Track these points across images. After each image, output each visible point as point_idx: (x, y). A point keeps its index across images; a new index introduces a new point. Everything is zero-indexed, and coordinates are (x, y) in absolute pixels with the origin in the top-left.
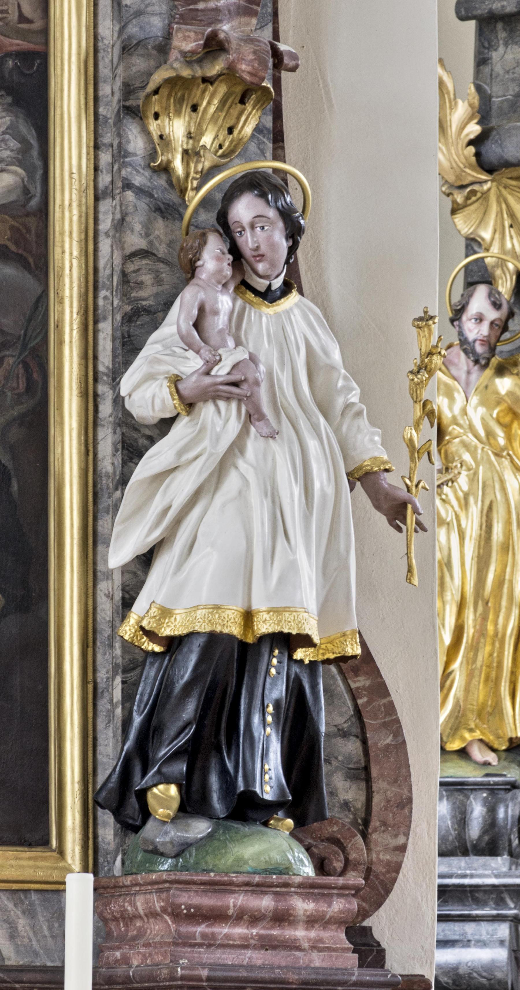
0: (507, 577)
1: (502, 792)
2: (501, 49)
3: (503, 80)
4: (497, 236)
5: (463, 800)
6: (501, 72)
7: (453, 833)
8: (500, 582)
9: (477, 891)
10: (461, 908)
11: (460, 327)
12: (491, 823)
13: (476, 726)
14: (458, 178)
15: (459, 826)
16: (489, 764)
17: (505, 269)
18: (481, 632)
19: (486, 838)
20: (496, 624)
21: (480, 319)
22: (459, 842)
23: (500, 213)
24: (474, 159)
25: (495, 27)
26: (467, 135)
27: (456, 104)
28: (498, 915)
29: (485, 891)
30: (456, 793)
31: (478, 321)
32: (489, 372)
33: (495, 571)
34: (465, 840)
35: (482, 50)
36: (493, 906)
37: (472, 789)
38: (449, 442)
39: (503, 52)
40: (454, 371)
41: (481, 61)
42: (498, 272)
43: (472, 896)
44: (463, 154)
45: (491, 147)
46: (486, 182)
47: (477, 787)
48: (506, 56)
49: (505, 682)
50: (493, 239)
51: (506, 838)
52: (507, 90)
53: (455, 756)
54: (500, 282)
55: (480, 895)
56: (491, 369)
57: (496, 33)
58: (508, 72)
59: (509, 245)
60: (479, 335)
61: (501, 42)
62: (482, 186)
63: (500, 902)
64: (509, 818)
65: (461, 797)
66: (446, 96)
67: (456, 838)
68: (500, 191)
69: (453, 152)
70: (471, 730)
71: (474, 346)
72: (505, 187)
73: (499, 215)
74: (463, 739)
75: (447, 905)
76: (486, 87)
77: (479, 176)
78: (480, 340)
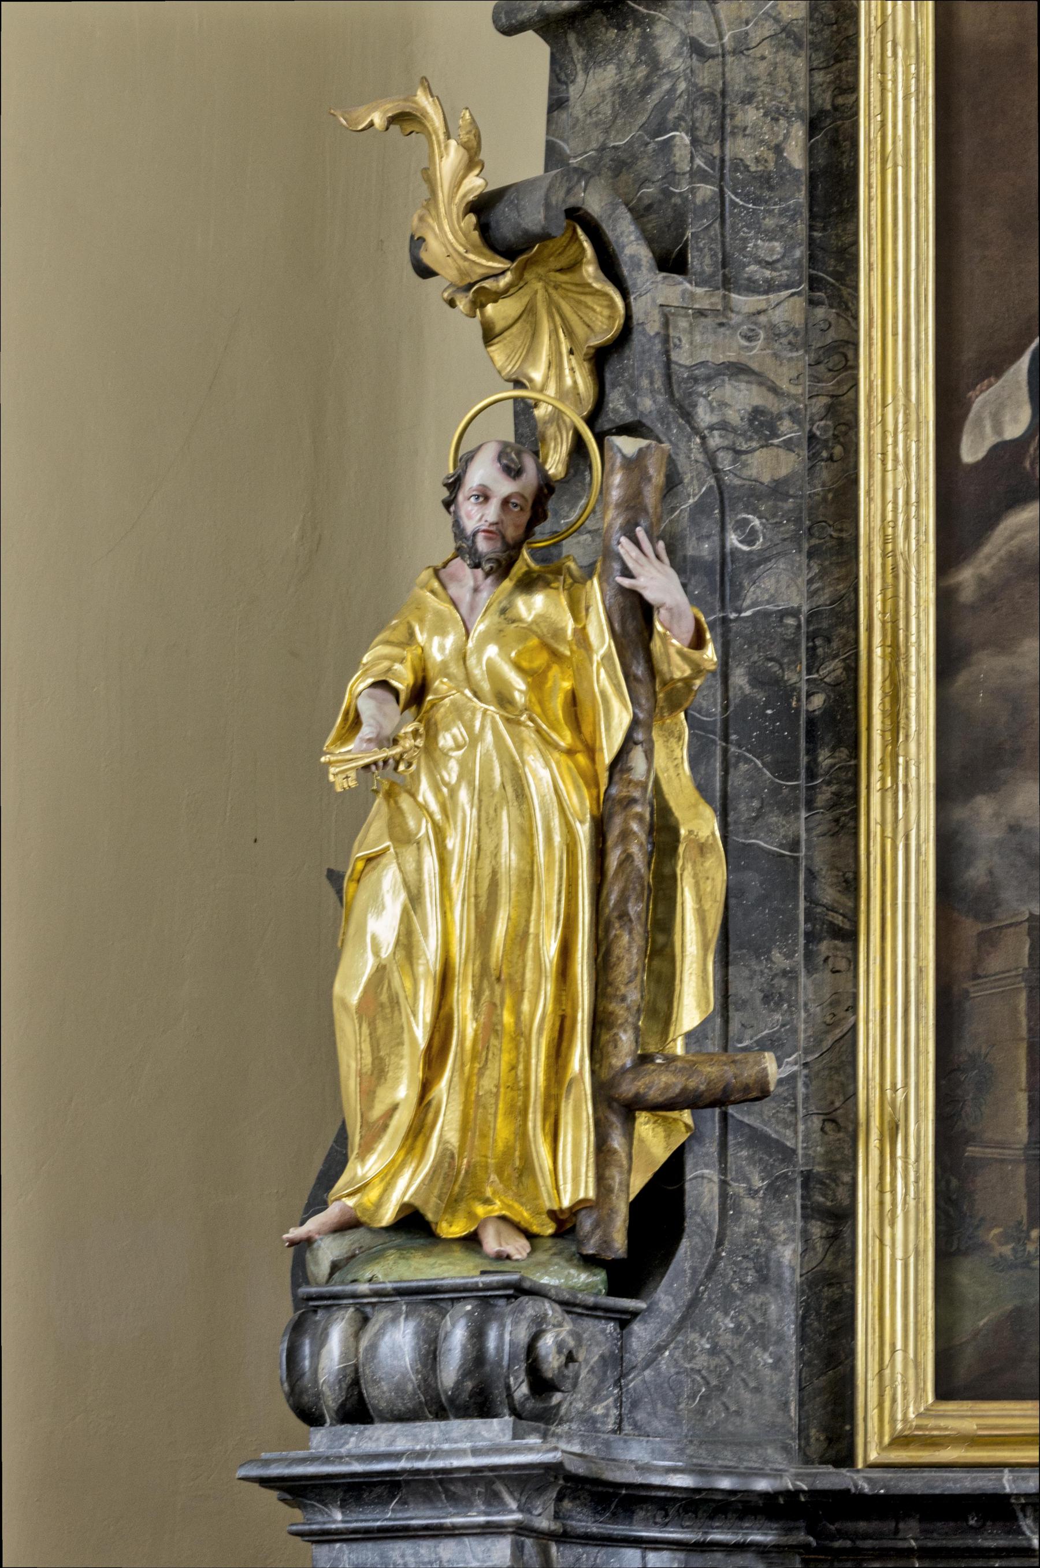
0: (532, 930)
1: (502, 1302)
2: (580, 78)
3: (583, 129)
4: (553, 372)
5: (432, 1319)
6: (581, 116)
7: (413, 1377)
8: (520, 937)
9: (452, 1481)
10: (429, 1513)
11: (455, 512)
12: (477, 1359)
13: (494, 1193)
14: (462, 273)
15: (424, 1366)
16: (508, 1257)
17: (561, 422)
18: (491, 1029)
19: (469, 1385)
20: (517, 1013)
21: (484, 496)
22: (425, 1393)
23: (554, 332)
24: (475, 235)
25: (566, 42)
26: (464, 196)
27: (447, 146)
28: (488, 1525)
29: (464, 1480)
30: (423, 1308)
31: (481, 499)
32: (507, 584)
33: (509, 918)
34: (436, 1388)
35: (557, 85)
36: (483, 1508)
37: (452, 1300)
38: (433, 705)
39: (583, 83)
40: (453, 590)
41: (557, 104)
42: (551, 431)
43: (446, 1491)
44: (460, 228)
45: (504, 211)
46: (503, 273)
47: (459, 1293)
48: (587, 89)
49: (535, 1112)
50: (547, 378)
51: (501, 1384)
52: (588, 142)
53: (456, 1247)
54: (552, 445)
55: (457, 1489)
56: (511, 580)
57: (570, 52)
58: (590, 113)
59: (569, 381)
60: (483, 522)
61: (579, 66)
62: (497, 281)
63: (493, 1499)
64: (507, 1348)
65: (431, 1314)
66: (434, 137)
67: (419, 1387)
68: (549, 295)
69: (447, 228)
70: (487, 1201)
71: (474, 542)
72: (556, 287)
73: (554, 337)
74: (471, 1215)
75: (407, 1510)
76: (561, 143)
77: (490, 264)
78: (484, 531)
